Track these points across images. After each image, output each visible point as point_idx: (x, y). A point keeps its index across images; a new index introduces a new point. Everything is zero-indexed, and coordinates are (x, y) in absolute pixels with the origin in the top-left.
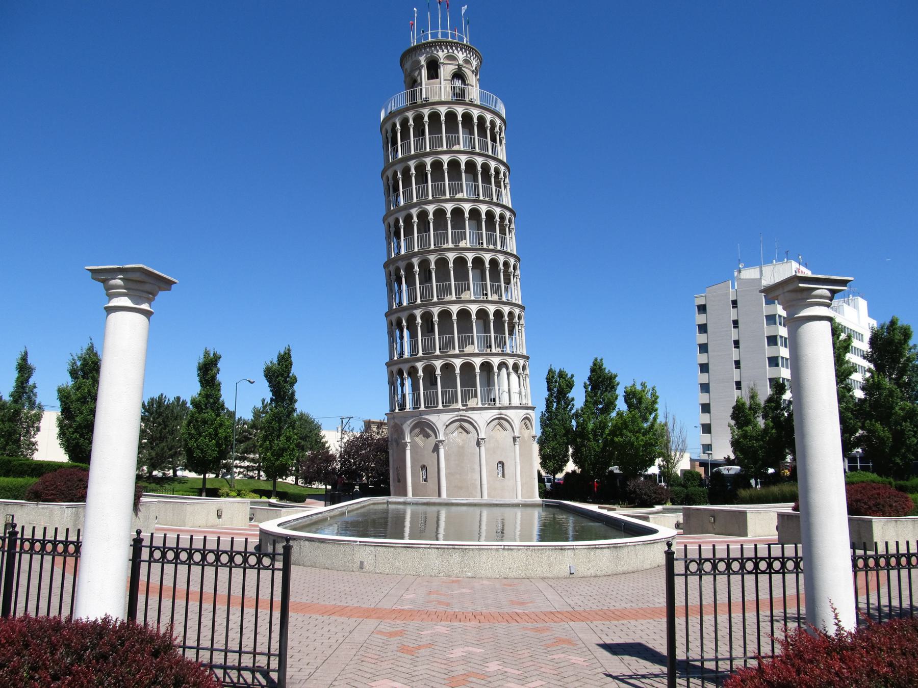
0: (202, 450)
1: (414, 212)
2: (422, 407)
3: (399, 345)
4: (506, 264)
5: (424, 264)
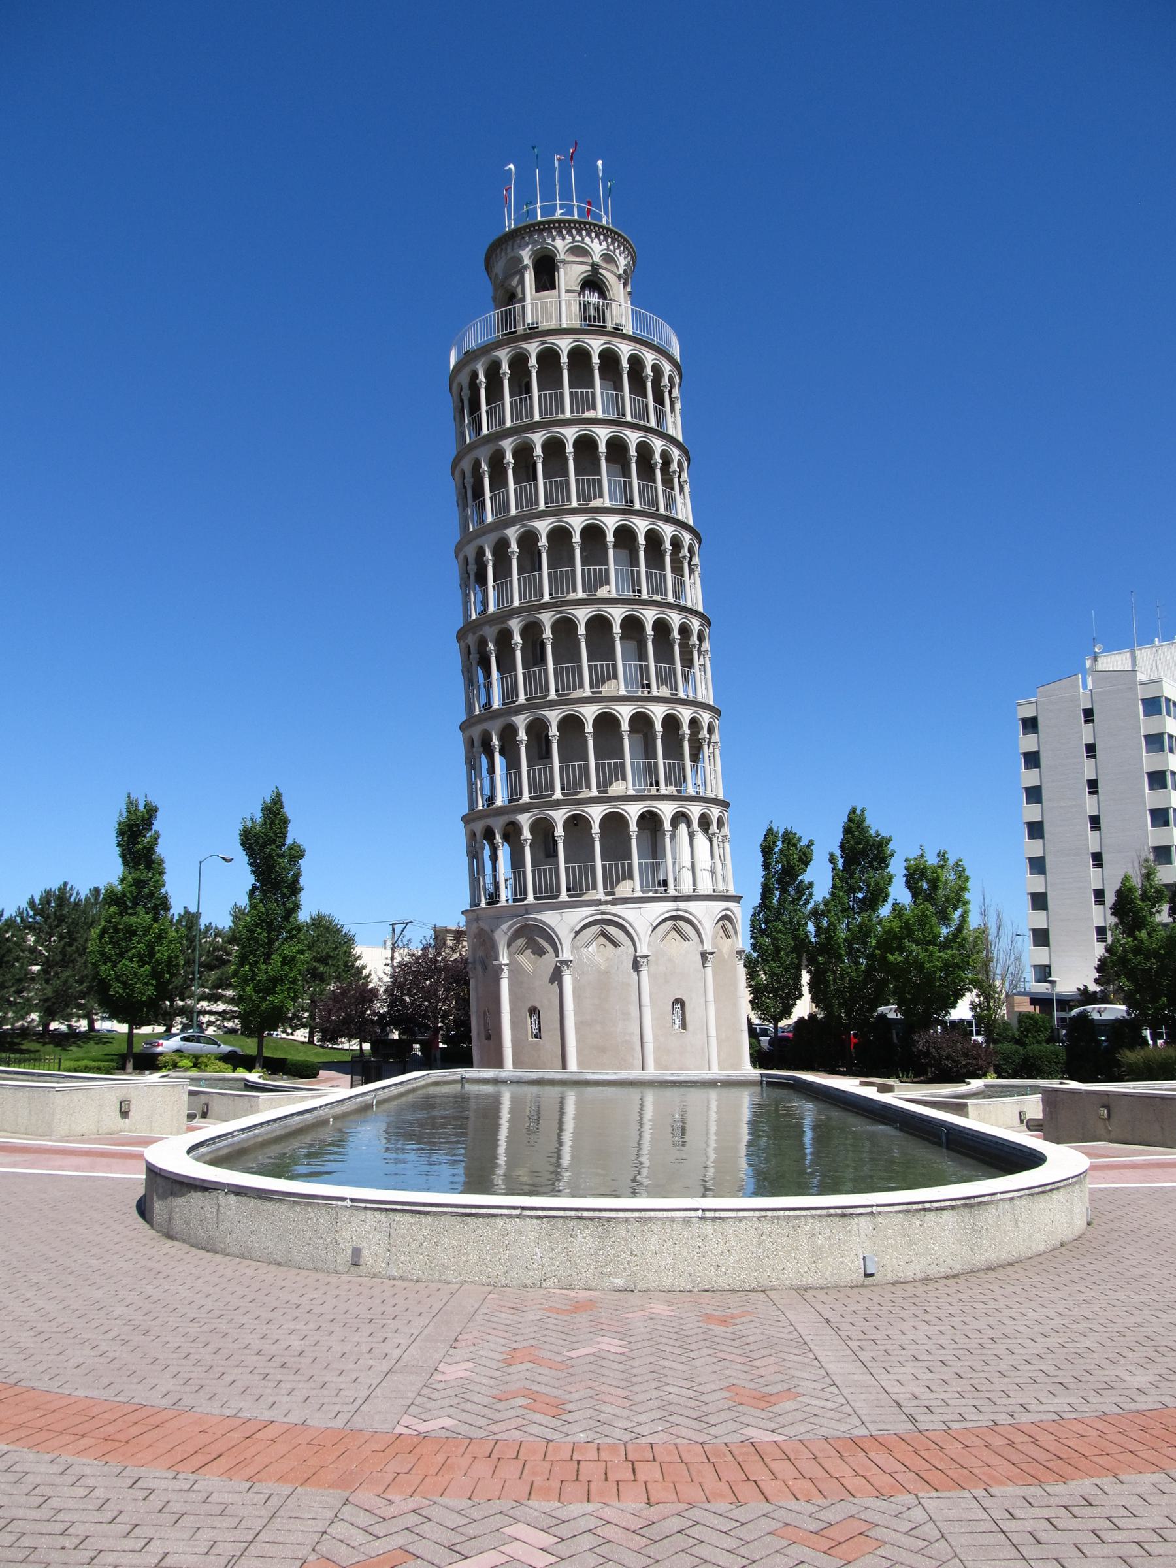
0: (124, 983)
1: (513, 533)
2: (530, 899)
3: (487, 782)
5: (532, 630)
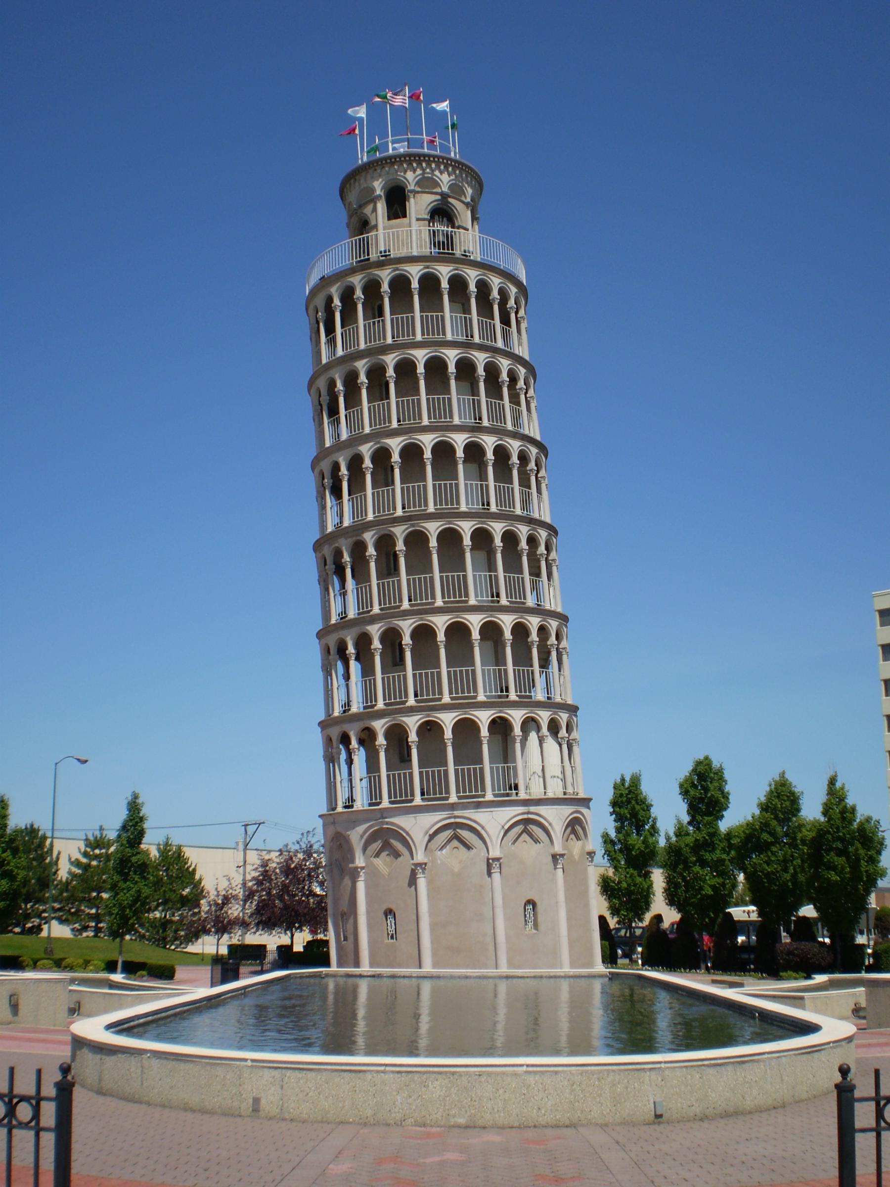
2: (385, 803)
4: (532, 541)
